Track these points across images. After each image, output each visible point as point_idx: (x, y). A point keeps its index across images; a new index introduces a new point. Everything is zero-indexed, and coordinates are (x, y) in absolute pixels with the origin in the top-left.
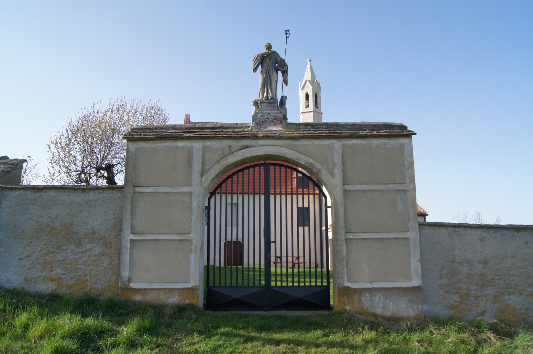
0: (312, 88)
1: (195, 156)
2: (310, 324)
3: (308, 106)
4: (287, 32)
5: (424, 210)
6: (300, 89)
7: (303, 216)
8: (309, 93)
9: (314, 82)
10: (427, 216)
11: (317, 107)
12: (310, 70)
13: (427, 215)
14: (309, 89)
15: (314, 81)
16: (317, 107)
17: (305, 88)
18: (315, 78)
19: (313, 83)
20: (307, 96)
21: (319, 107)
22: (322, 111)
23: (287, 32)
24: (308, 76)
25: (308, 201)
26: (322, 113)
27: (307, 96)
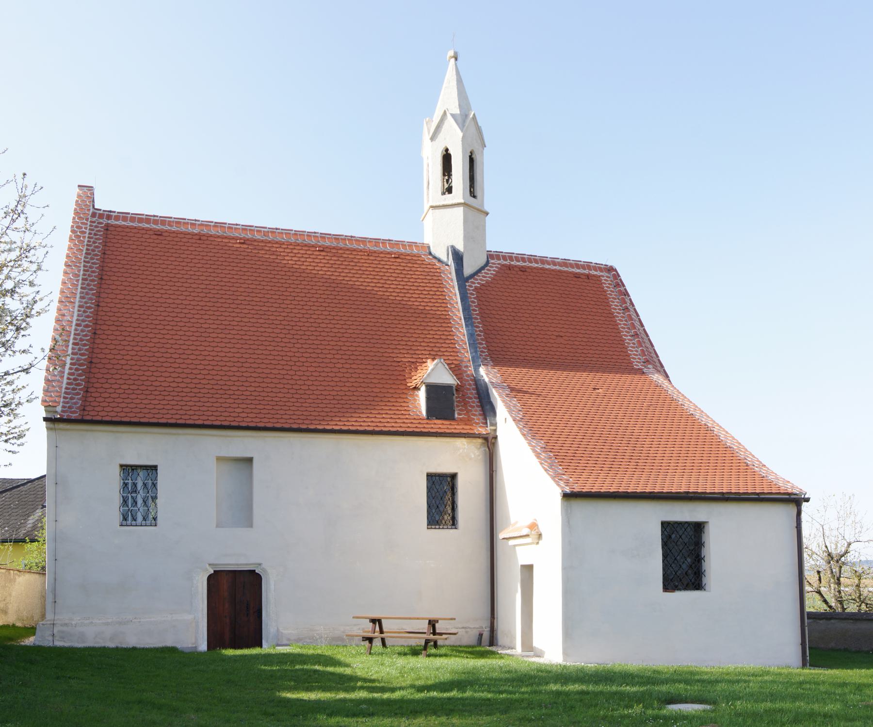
0: (460, 134)
1: (319, 652)
2: (417, 712)
3: (449, 190)
4: (24, 174)
5: (789, 486)
6: (427, 137)
7: (441, 493)
8: (451, 151)
9: (465, 119)
10: (804, 504)
11: (473, 194)
12: (454, 83)
13: (807, 500)
14: (453, 139)
15: (467, 116)
16: (473, 194)
17: (441, 136)
18: (469, 109)
19: (464, 121)
20: (447, 158)
21: (478, 193)
22: (486, 208)
23: (24, 174)
24: (448, 100)
25: (455, 456)
26: (487, 214)
27: (447, 158)
